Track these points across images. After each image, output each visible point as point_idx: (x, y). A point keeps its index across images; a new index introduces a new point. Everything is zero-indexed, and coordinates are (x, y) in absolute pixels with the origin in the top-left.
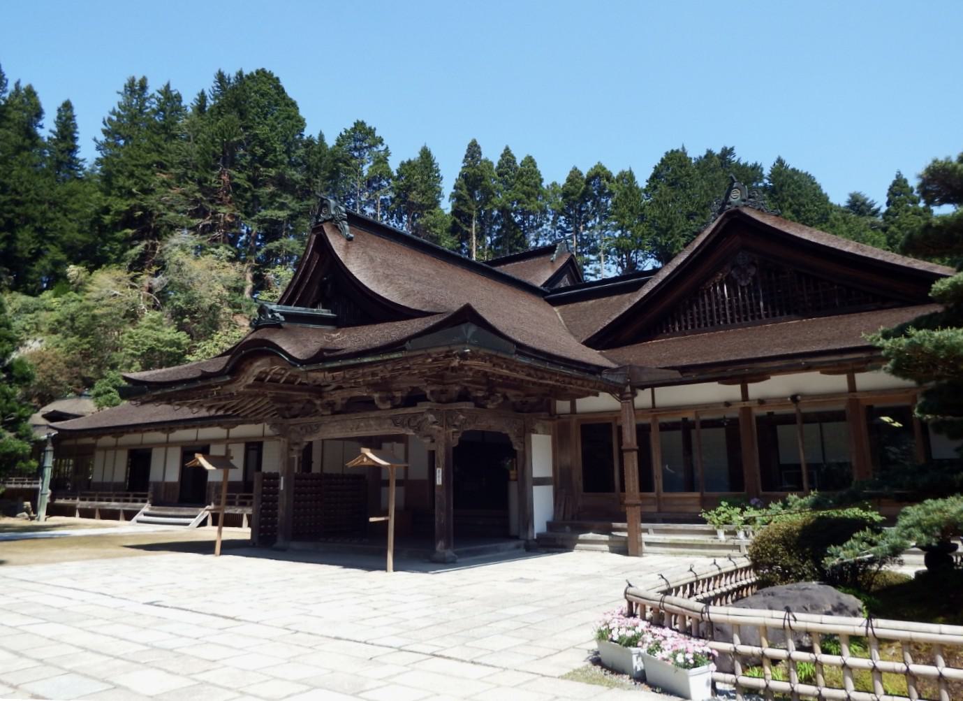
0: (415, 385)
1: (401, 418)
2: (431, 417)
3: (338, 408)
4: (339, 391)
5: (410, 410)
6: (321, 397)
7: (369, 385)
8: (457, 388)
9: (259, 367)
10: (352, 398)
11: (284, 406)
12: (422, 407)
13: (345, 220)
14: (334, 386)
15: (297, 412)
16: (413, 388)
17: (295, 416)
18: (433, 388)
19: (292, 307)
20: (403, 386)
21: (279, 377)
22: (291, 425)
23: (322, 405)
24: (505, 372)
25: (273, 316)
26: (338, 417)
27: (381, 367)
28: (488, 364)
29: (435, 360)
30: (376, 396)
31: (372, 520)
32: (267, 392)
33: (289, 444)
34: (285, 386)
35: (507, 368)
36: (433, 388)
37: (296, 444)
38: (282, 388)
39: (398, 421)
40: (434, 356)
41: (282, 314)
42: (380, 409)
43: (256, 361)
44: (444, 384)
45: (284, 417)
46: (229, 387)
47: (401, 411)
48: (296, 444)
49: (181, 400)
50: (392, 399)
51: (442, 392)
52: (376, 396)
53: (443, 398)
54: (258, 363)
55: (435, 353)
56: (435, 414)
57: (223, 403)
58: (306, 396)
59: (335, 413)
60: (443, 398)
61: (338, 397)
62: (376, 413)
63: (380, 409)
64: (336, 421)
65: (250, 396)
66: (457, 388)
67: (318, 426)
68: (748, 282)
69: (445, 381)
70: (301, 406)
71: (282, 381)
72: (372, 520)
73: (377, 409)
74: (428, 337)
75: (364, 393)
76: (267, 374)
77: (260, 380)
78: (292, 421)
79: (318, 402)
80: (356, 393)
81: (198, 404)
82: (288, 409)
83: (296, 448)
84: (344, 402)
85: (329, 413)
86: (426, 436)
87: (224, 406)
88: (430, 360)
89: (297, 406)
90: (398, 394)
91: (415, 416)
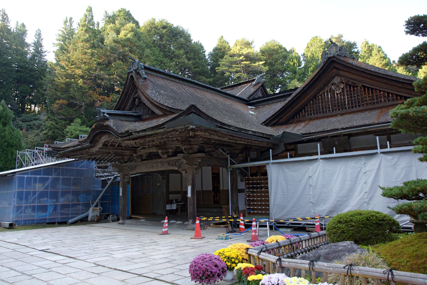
0: (178, 146)
1: (172, 162)
2: (185, 162)
3: (144, 158)
4: (144, 150)
5: (175, 158)
6: (136, 153)
7: (157, 146)
8: (197, 147)
9: (104, 139)
10: (150, 153)
11: (120, 157)
12: (180, 156)
13: (142, 69)
14: (141, 147)
15: (126, 161)
16: (177, 147)
17: (126, 162)
18: (185, 147)
19: (113, 110)
20: (173, 146)
21: (115, 144)
22: (123, 166)
23: (136, 157)
24: (217, 137)
25: (104, 115)
26: (144, 162)
27: (156, 137)
28: (207, 134)
29: (180, 132)
30: (160, 151)
31: (334, 148)
32: (111, 151)
33: (123, 175)
34: (118, 148)
35: (217, 136)
36: (185, 147)
37: (127, 175)
38: (116, 149)
39: (170, 163)
40: (180, 130)
41: (108, 114)
42: (162, 158)
43: (102, 136)
44: (191, 145)
45: (121, 163)
46: (91, 149)
47: (172, 158)
48: (127, 175)
49: (368, 131)
50: (168, 153)
51: (190, 149)
52: (160, 151)
53: (190, 151)
54: (103, 138)
55: (180, 129)
56: (186, 160)
57: (94, 157)
58: (128, 153)
59: (142, 160)
60: (190, 151)
61: (144, 152)
62: (161, 160)
63: (162, 158)
64: (143, 164)
65: (106, 153)
66: (197, 147)
67: (135, 167)
68: (340, 91)
69: (191, 144)
70: (128, 157)
71: (116, 145)
72: (334, 148)
73: (160, 158)
74: (174, 121)
75: (154, 150)
76: (109, 142)
77: (105, 145)
78: (124, 164)
79: (135, 155)
80: (151, 151)
81: (83, 158)
82: (123, 159)
83: (126, 177)
84: (147, 155)
85: (140, 160)
86: (183, 170)
87: (95, 158)
88: (178, 133)
89: (126, 157)
90: (170, 151)
91: (178, 160)
